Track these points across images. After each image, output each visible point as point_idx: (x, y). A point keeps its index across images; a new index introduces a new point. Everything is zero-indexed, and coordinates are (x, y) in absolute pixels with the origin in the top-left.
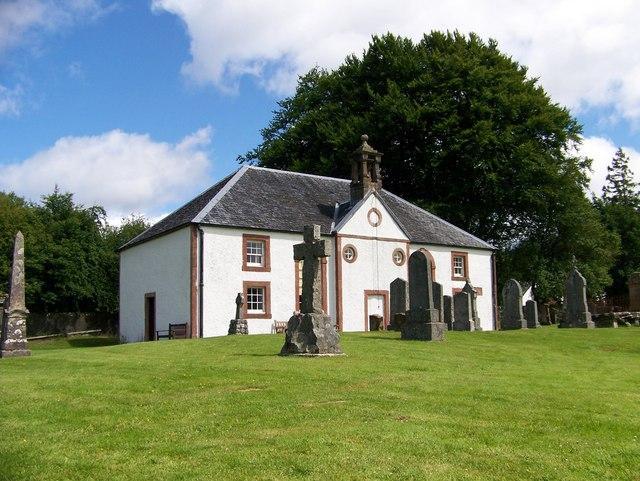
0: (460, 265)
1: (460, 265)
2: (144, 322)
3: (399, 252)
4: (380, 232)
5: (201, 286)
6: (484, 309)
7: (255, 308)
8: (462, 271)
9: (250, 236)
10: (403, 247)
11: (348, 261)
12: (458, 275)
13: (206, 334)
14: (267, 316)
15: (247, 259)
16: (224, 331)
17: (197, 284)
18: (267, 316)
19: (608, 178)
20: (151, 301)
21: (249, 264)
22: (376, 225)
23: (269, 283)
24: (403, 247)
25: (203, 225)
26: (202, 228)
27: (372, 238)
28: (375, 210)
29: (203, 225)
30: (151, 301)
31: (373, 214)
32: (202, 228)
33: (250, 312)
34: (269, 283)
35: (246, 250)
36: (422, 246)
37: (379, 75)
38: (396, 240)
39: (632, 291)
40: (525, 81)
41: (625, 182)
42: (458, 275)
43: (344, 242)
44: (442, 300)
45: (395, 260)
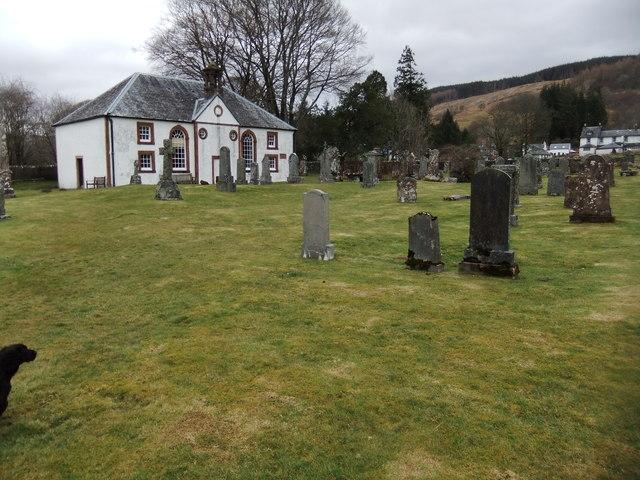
0: (272, 137)
1: (272, 137)
3: (233, 132)
4: (222, 120)
9: (143, 124)
10: (236, 129)
15: (140, 137)
16: (127, 181)
17: (110, 152)
19: (399, 69)
20: (80, 162)
22: (218, 116)
24: (236, 129)
26: (113, 119)
30: (80, 162)
32: (113, 119)
33: (174, 169)
35: (139, 132)
39: (4, 137)
40: (391, 88)
41: (411, 72)
43: (200, 126)
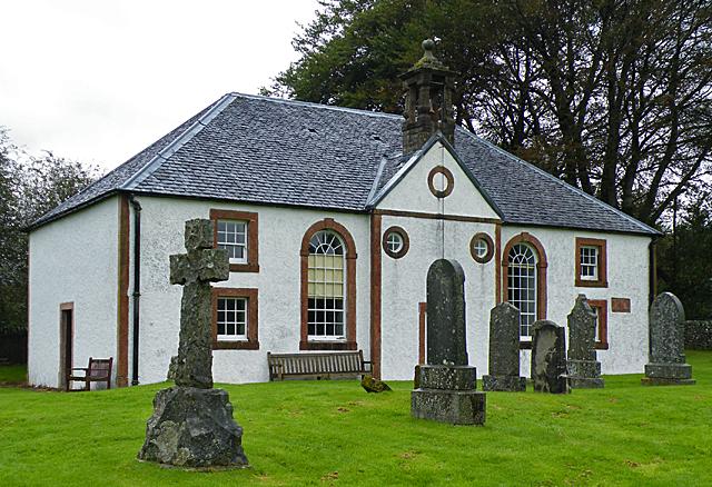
0: (591, 261)
1: (591, 261)
2: (58, 349)
3: (482, 238)
4: (450, 206)
5: (137, 295)
6: (626, 349)
7: (231, 332)
8: (595, 270)
11: (391, 254)
12: (587, 278)
13: (142, 381)
14: (253, 345)
15: (581, 270)
18: (253, 345)
20: (67, 315)
21: (583, 278)
22: (440, 195)
23: (255, 291)
25: (141, 194)
27: (439, 217)
28: (444, 171)
29: (141, 194)
30: (67, 315)
31: (438, 176)
33: (221, 338)
34: (255, 291)
36: (524, 230)
37: (600, 59)
38: (477, 220)
42: (587, 278)
43: (387, 223)
44: (302, 352)
45: (474, 253)
